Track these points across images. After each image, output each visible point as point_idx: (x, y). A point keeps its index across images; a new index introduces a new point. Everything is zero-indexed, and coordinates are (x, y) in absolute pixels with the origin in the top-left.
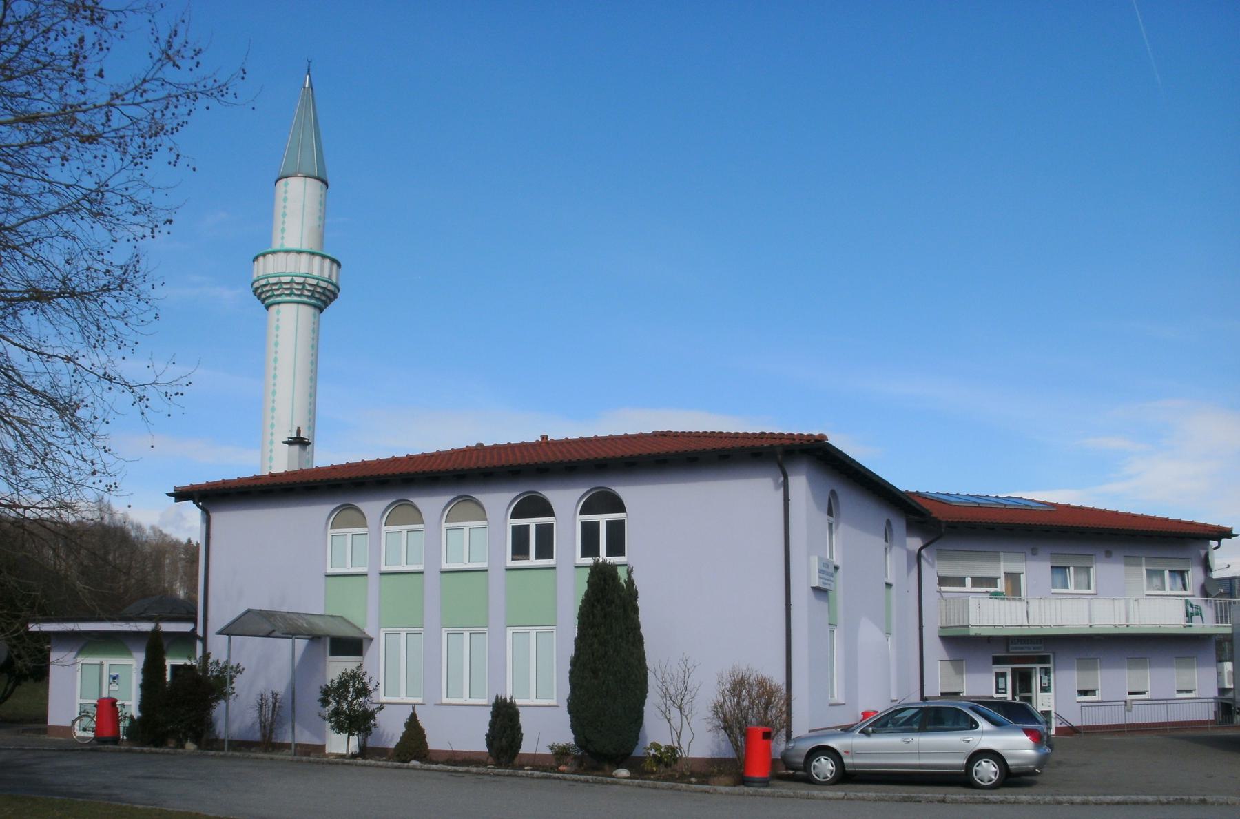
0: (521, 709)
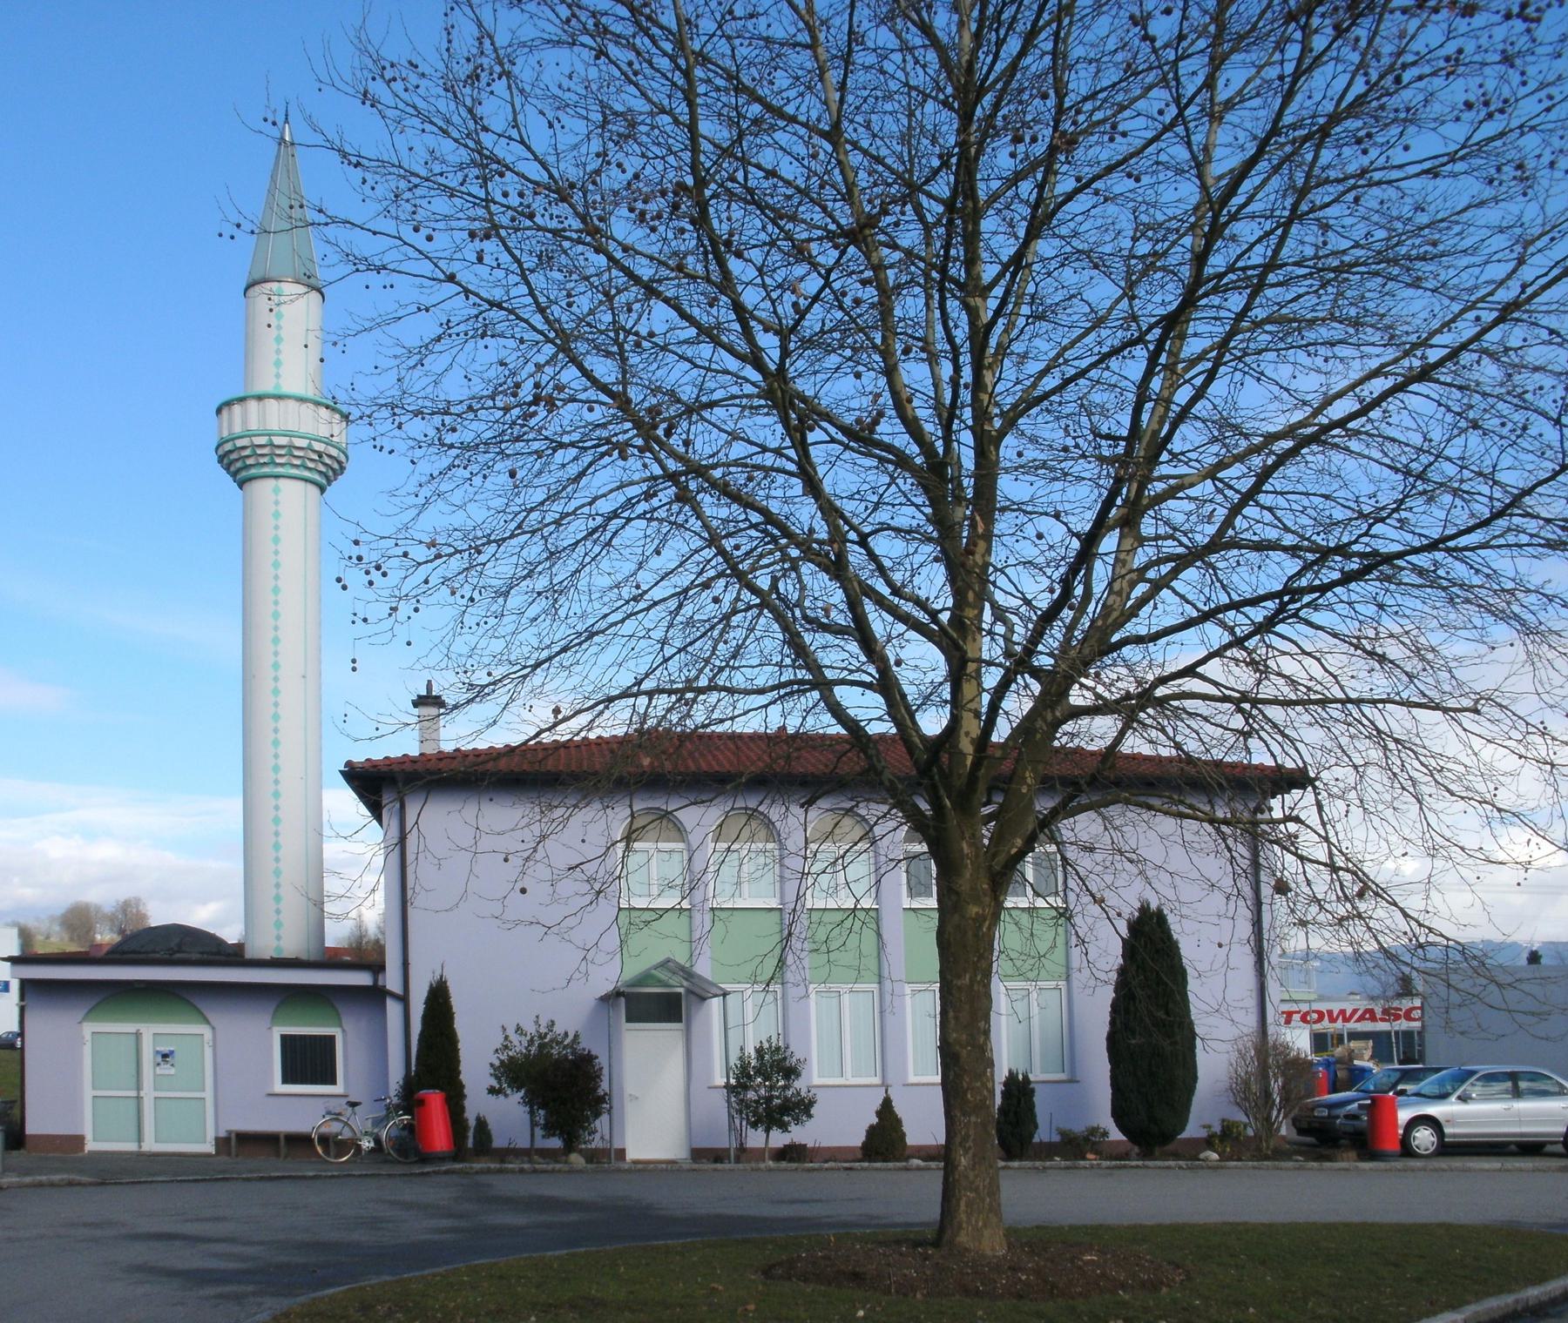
0: (1038, 1088)
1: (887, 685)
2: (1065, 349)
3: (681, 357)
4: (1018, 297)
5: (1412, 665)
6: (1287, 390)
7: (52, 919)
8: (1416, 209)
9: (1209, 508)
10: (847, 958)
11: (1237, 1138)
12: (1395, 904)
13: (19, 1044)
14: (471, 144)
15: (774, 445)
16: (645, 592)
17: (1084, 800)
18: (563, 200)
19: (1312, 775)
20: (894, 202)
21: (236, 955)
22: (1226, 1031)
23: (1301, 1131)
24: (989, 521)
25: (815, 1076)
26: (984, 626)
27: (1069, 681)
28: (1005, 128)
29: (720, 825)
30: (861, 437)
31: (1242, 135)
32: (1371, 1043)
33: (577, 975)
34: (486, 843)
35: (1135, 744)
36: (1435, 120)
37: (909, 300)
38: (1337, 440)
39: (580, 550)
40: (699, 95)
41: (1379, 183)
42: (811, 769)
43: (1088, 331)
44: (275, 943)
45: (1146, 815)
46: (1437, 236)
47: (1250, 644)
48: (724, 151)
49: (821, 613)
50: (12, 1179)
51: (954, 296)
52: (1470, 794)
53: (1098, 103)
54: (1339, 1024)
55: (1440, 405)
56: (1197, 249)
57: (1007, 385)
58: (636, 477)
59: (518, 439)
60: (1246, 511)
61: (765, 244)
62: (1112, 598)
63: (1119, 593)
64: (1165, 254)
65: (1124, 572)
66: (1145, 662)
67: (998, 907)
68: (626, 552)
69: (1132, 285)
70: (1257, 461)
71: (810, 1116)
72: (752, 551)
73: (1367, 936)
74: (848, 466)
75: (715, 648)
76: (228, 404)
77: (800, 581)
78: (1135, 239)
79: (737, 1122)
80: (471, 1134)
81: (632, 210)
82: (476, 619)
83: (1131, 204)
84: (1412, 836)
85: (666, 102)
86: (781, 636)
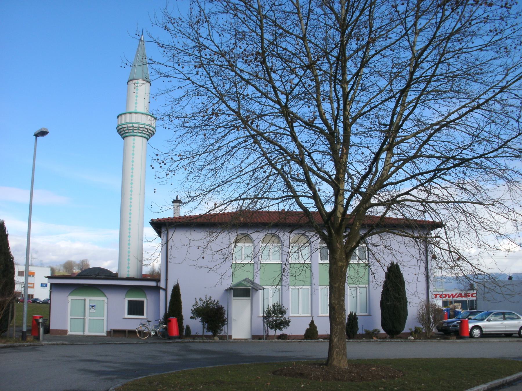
0: (358, 317)
1: (315, 197)
2: (371, 99)
3: (256, 101)
4: (357, 84)
5: (475, 191)
7: (61, 265)
8: (476, 60)
9: (414, 145)
11: (420, 332)
12: (469, 262)
14: (196, 41)
15: (283, 127)
16: (243, 170)
17: (374, 231)
18: (223, 57)
19: (444, 224)
20: (321, 57)
23: (439, 330)
24: (347, 149)
25: (290, 314)
26: (345, 180)
27: (371, 196)
28: (354, 36)
29: (264, 238)
30: (309, 125)
31: (425, 39)
33: (219, 283)
35: (390, 215)
36: (481, 35)
38: (452, 126)
39: (224, 157)
40: (264, 27)
41: (465, 52)
42: (292, 222)
43: (378, 94)
45: (393, 236)
46: (482, 68)
47: (426, 185)
48: (271, 43)
49: (296, 176)
51: (338, 84)
54: (451, 298)
55: (483, 116)
56: (411, 71)
57: (354, 109)
58: (242, 136)
59: (207, 125)
61: (282, 69)
62: (384, 171)
63: (386, 170)
64: (401, 72)
65: (388, 164)
66: (394, 190)
67: (348, 263)
69: (391, 81)
70: (428, 132)
71: (289, 326)
72: (276, 157)
73: (460, 272)
75: (264, 186)
76: (121, 115)
77: (290, 166)
78: (392, 68)
79: (266, 327)
80: (184, 331)
81: (243, 59)
82: (192, 177)
83: (391, 58)
84: (474, 242)
85: (254, 29)
86: (284, 183)
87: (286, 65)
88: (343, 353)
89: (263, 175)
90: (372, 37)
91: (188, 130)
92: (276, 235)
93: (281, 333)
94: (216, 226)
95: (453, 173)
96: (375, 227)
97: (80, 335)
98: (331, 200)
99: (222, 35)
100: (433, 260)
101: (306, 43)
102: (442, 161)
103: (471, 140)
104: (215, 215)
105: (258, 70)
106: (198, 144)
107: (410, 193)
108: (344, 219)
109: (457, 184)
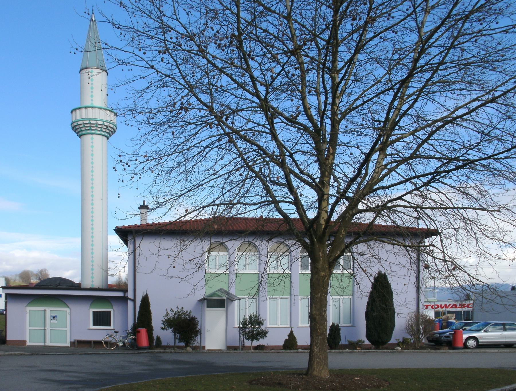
1: (297, 202)
2: (365, 91)
3: (231, 94)
4: (349, 74)
5: (477, 196)
6: (442, 105)
7: (16, 275)
8: (498, 44)
9: (411, 145)
10: (280, 288)
11: (408, 343)
12: (466, 272)
13: (5, 313)
14: (159, 21)
15: (262, 123)
16: (217, 172)
17: (361, 239)
18: (192, 40)
19: (440, 231)
20: (308, 41)
21: (78, 287)
22: (405, 311)
23: (429, 341)
24: (334, 149)
25: (268, 324)
26: (331, 183)
27: (358, 201)
28: (350, 15)
29: (240, 247)
30: (292, 121)
31: (436, 18)
32: (455, 315)
33: (191, 293)
34: (162, 252)
35: (379, 221)
36: (509, 13)
37: (312, 75)
38: (458, 122)
39: (196, 158)
40: (241, 3)
41: (485, 35)
42: (270, 229)
43: (373, 85)
44: (91, 283)
45: (382, 244)
46: (504, 54)
47: (422, 189)
48: (249, 23)
49: (276, 179)
50: (2, 353)
51: (327, 73)
52: (495, 238)
53: (385, 6)
54: (444, 309)
55: (497, 111)
56: (415, 57)
57: (343, 103)
58: (215, 134)
59: (175, 121)
60: (424, 146)
61: (262, 55)
62: (375, 174)
63: (377, 173)
64: (403, 59)
65: (379, 166)
66: (385, 195)
67: (331, 273)
68: (211, 159)
69: (390, 70)
70: (429, 129)
71: (266, 336)
72: (253, 159)
73: (455, 282)
74: (287, 131)
75: (240, 190)
76: (75, 110)
77: (269, 168)
78: (393, 54)
79: (242, 338)
80: (155, 341)
81: (216, 43)
82: (160, 181)
83: (393, 42)
84: (473, 251)
85: (229, 6)
86: (262, 187)
87: (266, 51)
88: (324, 363)
89: (239, 178)
90: (372, 16)
91: (154, 127)
92: (254, 243)
93: (258, 344)
94: (188, 234)
95: (455, 176)
96: (362, 235)
97: (40, 346)
98: (314, 206)
99: (190, 14)
100: (425, 270)
101: (291, 23)
102: (443, 162)
103: (480, 138)
104: (186, 222)
105: (233, 57)
106: (166, 143)
107: (403, 198)
108: (329, 226)
109: (458, 188)
